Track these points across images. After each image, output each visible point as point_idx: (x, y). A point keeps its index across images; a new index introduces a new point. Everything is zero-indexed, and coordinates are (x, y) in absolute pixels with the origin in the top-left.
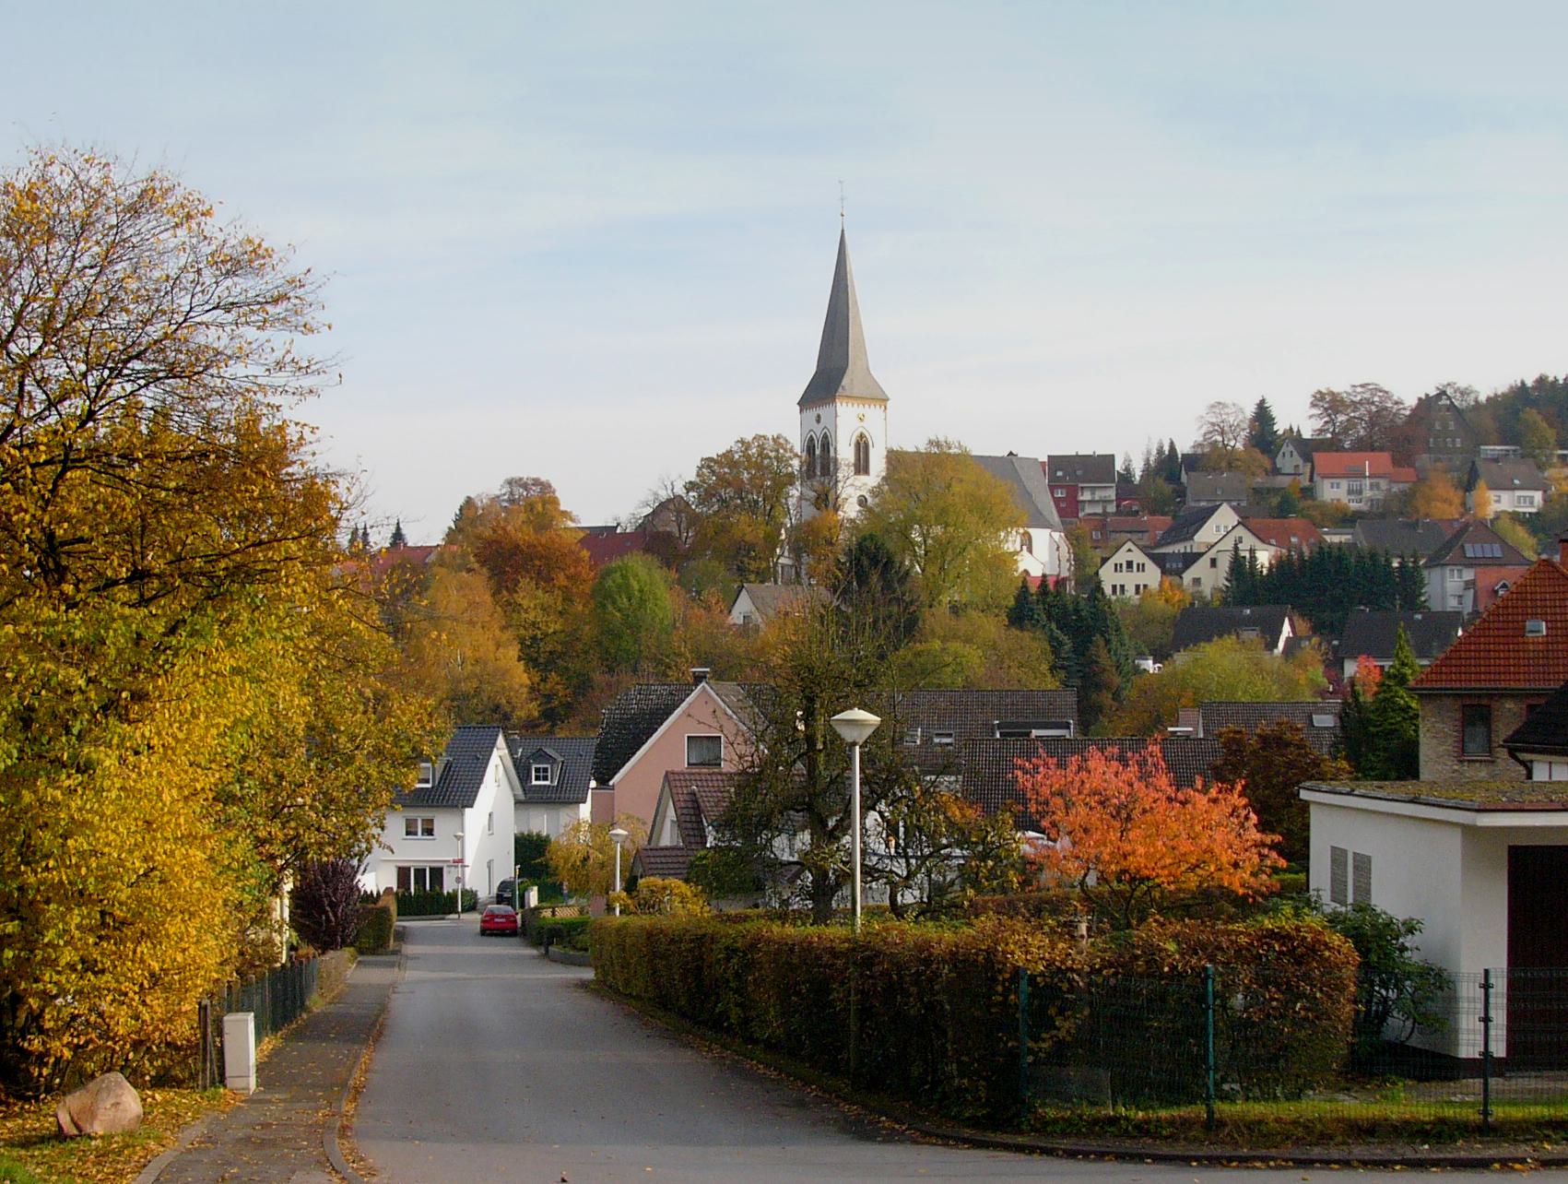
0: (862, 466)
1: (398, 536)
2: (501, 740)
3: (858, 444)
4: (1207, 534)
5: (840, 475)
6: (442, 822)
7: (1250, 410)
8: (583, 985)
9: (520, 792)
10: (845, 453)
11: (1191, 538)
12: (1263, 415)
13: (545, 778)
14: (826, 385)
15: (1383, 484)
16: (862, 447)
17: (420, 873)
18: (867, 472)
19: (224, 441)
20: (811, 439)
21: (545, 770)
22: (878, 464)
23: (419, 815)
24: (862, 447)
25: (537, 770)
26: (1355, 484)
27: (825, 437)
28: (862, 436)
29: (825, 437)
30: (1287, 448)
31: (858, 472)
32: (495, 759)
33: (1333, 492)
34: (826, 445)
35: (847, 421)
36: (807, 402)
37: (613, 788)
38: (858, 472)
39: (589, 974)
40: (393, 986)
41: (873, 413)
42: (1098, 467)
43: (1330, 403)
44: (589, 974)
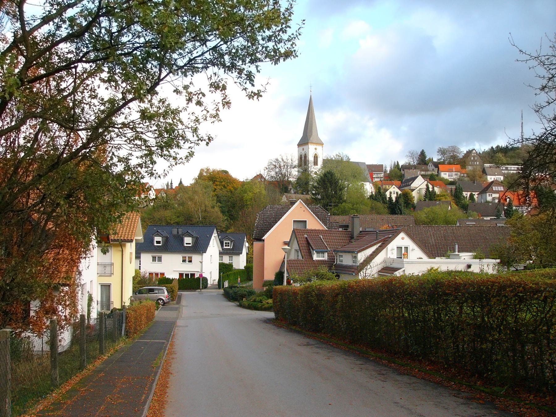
0: (316, 163)
1: (181, 183)
2: (215, 234)
3: (315, 157)
4: (414, 185)
5: (310, 165)
6: (196, 258)
7: (419, 153)
8: (268, 321)
9: (221, 249)
10: (311, 158)
11: (410, 185)
12: (423, 154)
13: (228, 246)
14: (304, 142)
15: (459, 174)
16: (316, 157)
17: (187, 275)
18: (317, 165)
20: (301, 155)
21: (228, 243)
22: (320, 162)
23: (187, 255)
24: (316, 157)
25: (226, 243)
26: (450, 174)
27: (305, 154)
28: (316, 154)
29: (305, 154)
30: (430, 164)
31: (314, 165)
33: (445, 175)
34: (305, 157)
35: (312, 150)
36: (299, 145)
37: (264, 240)
38: (314, 165)
39: (271, 315)
41: (319, 148)
42: (379, 168)
43: (442, 152)
44: (271, 315)
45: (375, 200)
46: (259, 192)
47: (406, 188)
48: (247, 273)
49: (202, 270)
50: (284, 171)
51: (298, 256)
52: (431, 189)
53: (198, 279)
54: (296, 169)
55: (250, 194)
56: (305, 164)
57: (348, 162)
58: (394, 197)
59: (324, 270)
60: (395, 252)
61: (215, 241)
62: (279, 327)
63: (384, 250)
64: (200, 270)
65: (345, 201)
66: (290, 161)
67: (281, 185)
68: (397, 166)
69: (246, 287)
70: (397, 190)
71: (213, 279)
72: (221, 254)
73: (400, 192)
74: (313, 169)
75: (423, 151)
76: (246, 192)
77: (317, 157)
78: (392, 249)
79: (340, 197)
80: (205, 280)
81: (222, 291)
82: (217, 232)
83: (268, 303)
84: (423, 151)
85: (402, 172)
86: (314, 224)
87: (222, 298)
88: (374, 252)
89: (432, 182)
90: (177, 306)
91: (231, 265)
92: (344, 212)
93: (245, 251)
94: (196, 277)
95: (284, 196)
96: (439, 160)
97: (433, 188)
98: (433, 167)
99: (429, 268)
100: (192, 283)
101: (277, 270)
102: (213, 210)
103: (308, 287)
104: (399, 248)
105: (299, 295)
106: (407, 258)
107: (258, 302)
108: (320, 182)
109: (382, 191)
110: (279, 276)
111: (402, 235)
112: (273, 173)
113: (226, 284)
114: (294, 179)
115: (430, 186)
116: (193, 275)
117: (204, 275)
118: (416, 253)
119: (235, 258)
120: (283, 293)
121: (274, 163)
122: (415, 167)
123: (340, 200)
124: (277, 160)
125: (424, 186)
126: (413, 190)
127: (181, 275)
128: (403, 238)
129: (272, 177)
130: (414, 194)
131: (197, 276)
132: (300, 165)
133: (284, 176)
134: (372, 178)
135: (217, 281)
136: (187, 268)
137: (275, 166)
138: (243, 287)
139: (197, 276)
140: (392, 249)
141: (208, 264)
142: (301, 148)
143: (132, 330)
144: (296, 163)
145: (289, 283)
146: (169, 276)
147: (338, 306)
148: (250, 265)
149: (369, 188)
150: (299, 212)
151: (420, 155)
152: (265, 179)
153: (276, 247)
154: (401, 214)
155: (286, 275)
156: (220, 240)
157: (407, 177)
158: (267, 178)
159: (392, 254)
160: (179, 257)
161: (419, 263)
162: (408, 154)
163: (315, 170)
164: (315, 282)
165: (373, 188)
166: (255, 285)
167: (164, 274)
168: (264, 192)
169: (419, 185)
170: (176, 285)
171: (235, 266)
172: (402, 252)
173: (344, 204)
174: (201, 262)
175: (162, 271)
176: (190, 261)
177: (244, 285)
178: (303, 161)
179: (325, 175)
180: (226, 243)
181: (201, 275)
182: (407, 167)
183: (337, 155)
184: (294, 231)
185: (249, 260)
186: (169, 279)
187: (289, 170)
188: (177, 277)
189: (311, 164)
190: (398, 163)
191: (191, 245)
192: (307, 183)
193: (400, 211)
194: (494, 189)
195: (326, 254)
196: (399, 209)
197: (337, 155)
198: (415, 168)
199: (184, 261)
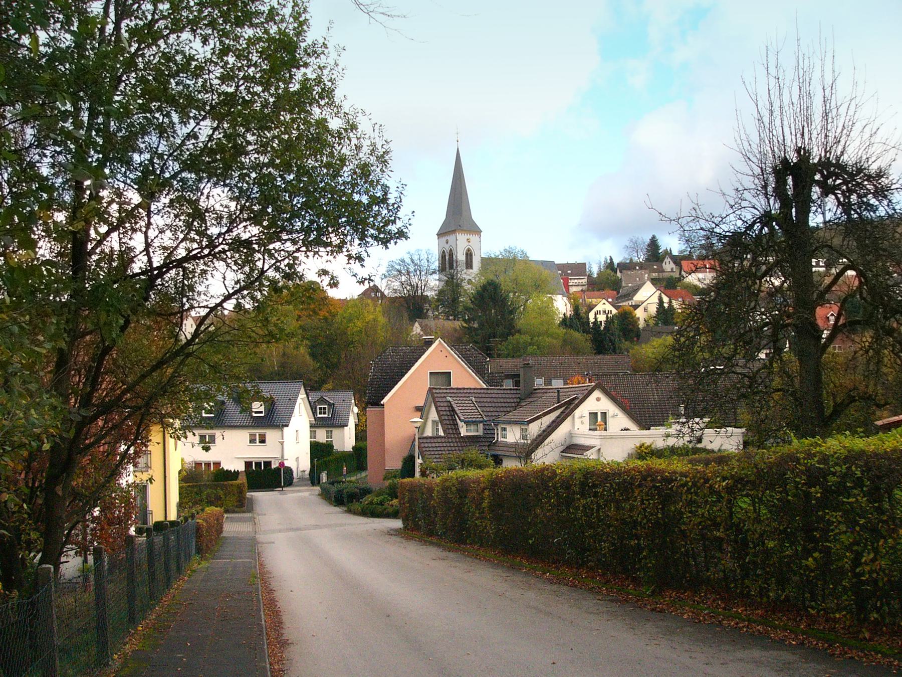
0: (469, 265)
3: (467, 254)
4: (639, 297)
6: (271, 435)
7: (648, 241)
10: (461, 257)
12: (653, 244)
13: (325, 413)
16: (469, 255)
17: (258, 464)
18: (471, 267)
19: (61, 16)
21: (325, 409)
23: (257, 432)
24: (469, 255)
25: (320, 409)
27: (451, 250)
28: (469, 250)
29: (451, 250)
30: (667, 260)
31: (467, 268)
32: (299, 401)
34: (451, 255)
36: (440, 235)
38: (467, 268)
40: (571, 435)
41: (473, 238)
42: (579, 269)
44: (398, 524)
45: (571, 327)
46: (374, 320)
47: (625, 304)
48: (358, 457)
49: (283, 457)
50: (415, 280)
51: (437, 430)
52: (666, 305)
53: (278, 470)
54: (436, 276)
55: (359, 324)
56: (451, 267)
57: (526, 261)
58: (602, 318)
59: (473, 453)
60: (587, 420)
61: (302, 406)
62: (409, 538)
63: (570, 418)
64: (279, 456)
65: (519, 331)
66: (424, 263)
67: (412, 305)
68: (610, 265)
69: (357, 481)
70: (609, 307)
71: (301, 469)
72: (314, 426)
73: (614, 311)
74: (465, 276)
75: (654, 237)
76: (350, 320)
77: (471, 255)
78: (582, 417)
79: (510, 324)
80: (289, 471)
81: (317, 489)
82: (306, 390)
83: (392, 506)
84: (654, 237)
85: (619, 274)
86: (464, 377)
87: (319, 500)
88: (553, 422)
89: (669, 292)
90: (249, 515)
91: (329, 447)
92: (516, 352)
93: (352, 421)
94: (273, 466)
95: (417, 324)
96: (681, 252)
97: (670, 302)
98: (672, 265)
99: (638, 445)
100: (268, 476)
101: (406, 454)
102: (295, 352)
103: (446, 480)
104: (593, 415)
105: (435, 492)
106: (603, 432)
107: (378, 504)
108: (476, 299)
109: (583, 310)
110: (409, 462)
111: (597, 394)
112: (396, 285)
113: (324, 477)
114: (433, 293)
115: (666, 299)
116: (268, 464)
117: (287, 464)
118: (618, 420)
119: (336, 432)
120: (413, 489)
121: (398, 267)
122: (642, 266)
123: (511, 329)
124: (403, 261)
125: (655, 299)
126: (636, 307)
127: (248, 464)
128: (598, 399)
129: (395, 291)
130: (639, 313)
131: (274, 466)
132: (442, 269)
133: (415, 288)
134: (567, 287)
135: (307, 472)
136: (258, 453)
137: (400, 272)
138: (351, 482)
139: (274, 466)
140: (582, 417)
141: (293, 445)
142: (444, 239)
143: (204, 547)
144: (436, 265)
145: (423, 474)
146: (228, 466)
147: (485, 504)
148: (361, 444)
149: (562, 306)
150: (439, 357)
151: (649, 245)
152: (382, 294)
153: (404, 414)
154: (614, 351)
155: (419, 461)
157: (627, 285)
158: (386, 293)
159: (582, 423)
160: (242, 436)
161: (623, 437)
162: (627, 243)
163: (471, 278)
164: (460, 473)
165: (569, 305)
166: (371, 477)
167: (219, 464)
168: (382, 320)
169: (648, 298)
170: (242, 480)
171: (337, 447)
172: (598, 421)
173: (517, 336)
174: (282, 443)
175: (216, 459)
176: (263, 441)
177: (353, 479)
178: (447, 262)
179: (484, 288)
180: (320, 409)
181: (282, 464)
182: (625, 266)
183: (505, 250)
184: (430, 389)
185: (361, 435)
186: (229, 472)
187: (423, 278)
188: (241, 468)
189: (462, 267)
190: (611, 259)
191: (263, 415)
192: (455, 300)
193: (613, 344)
195: (481, 426)
196: (611, 341)
197: (505, 250)
198: (641, 268)
199: (252, 441)
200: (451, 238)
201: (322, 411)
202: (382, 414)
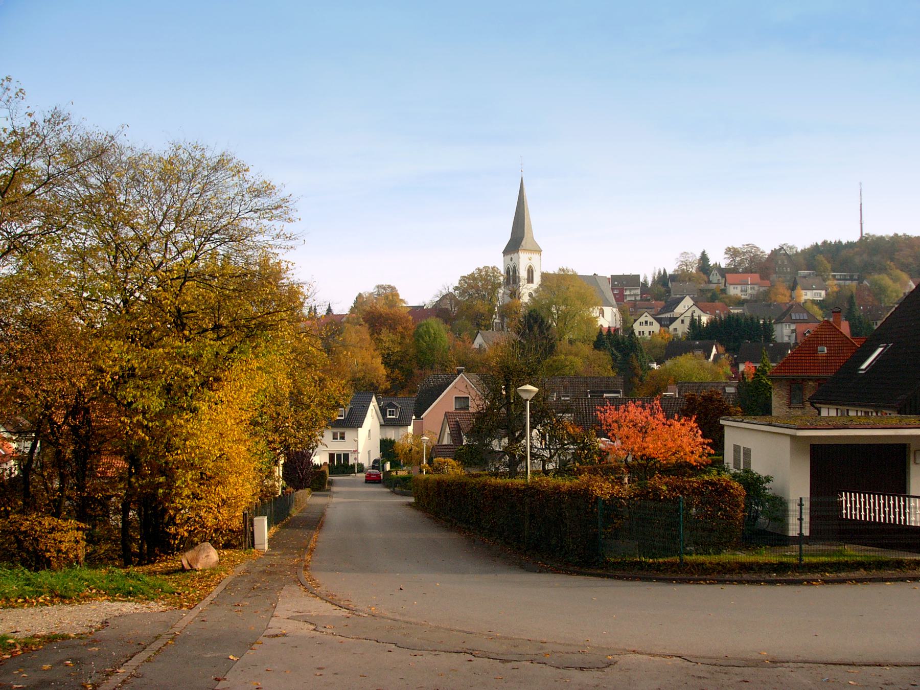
0: (530, 280)
2: (374, 399)
4: (679, 309)
6: (349, 434)
7: (698, 256)
8: (410, 504)
9: (382, 421)
10: (523, 274)
12: (704, 258)
14: (514, 245)
15: (756, 287)
16: (530, 272)
17: (339, 456)
18: (532, 282)
22: (537, 279)
23: (339, 431)
24: (530, 272)
26: (744, 287)
34: (515, 271)
35: (524, 260)
36: (506, 252)
38: (528, 282)
39: (412, 500)
40: (327, 505)
41: (535, 256)
42: (633, 280)
43: (733, 252)
44: (412, 500)
142: (509, 257)
156: (380, 408)
176: (343, 438)
189: (523, 282)
190: (665, 271)
194: (793, 318)
200: (514, 256)
201: (392, 413)
202: (422, 423)
